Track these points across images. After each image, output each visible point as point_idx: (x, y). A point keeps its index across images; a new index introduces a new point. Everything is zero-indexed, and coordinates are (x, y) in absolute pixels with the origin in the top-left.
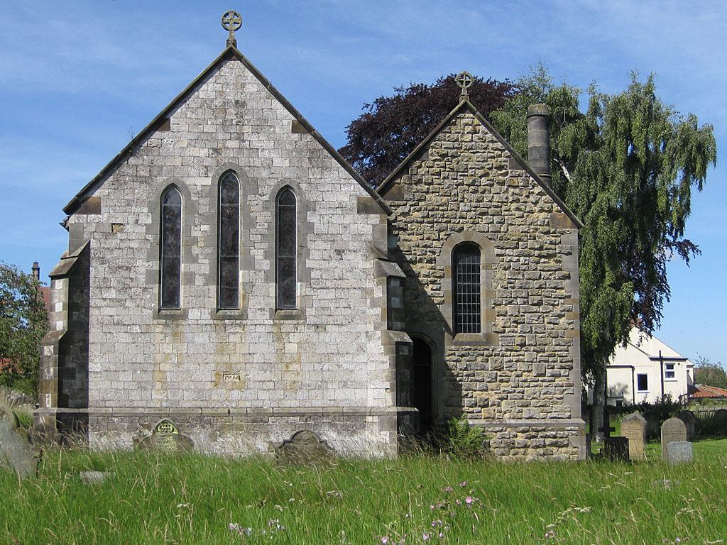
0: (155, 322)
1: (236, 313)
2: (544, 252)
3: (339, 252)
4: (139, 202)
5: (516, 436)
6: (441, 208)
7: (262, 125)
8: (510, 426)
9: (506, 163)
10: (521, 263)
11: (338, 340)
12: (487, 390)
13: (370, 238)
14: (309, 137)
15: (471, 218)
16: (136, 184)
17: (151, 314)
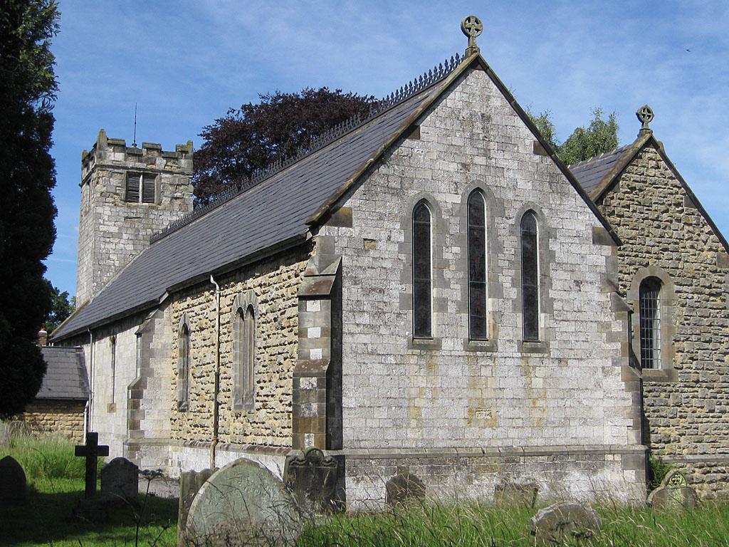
0: (410, 352)
1: (486, 344)
2: (714, 291)
3: (578, 283)
4: (392, 217)
5: (694, 472)
6: (631, 242)
7: (507, 143)
8: (689, 461)
9: (681, 201)
10: (694, 300)
11: (578, 375)
12: (669, 426)
13: (604, 270)
14: (549, 160)
15: (656, 253)
16: (388, 197)
17: (406, 344)
